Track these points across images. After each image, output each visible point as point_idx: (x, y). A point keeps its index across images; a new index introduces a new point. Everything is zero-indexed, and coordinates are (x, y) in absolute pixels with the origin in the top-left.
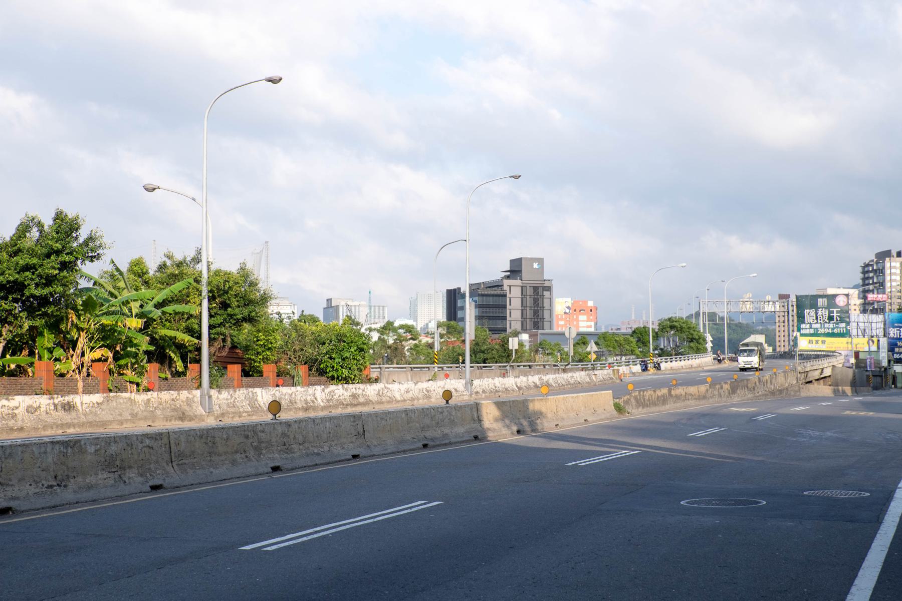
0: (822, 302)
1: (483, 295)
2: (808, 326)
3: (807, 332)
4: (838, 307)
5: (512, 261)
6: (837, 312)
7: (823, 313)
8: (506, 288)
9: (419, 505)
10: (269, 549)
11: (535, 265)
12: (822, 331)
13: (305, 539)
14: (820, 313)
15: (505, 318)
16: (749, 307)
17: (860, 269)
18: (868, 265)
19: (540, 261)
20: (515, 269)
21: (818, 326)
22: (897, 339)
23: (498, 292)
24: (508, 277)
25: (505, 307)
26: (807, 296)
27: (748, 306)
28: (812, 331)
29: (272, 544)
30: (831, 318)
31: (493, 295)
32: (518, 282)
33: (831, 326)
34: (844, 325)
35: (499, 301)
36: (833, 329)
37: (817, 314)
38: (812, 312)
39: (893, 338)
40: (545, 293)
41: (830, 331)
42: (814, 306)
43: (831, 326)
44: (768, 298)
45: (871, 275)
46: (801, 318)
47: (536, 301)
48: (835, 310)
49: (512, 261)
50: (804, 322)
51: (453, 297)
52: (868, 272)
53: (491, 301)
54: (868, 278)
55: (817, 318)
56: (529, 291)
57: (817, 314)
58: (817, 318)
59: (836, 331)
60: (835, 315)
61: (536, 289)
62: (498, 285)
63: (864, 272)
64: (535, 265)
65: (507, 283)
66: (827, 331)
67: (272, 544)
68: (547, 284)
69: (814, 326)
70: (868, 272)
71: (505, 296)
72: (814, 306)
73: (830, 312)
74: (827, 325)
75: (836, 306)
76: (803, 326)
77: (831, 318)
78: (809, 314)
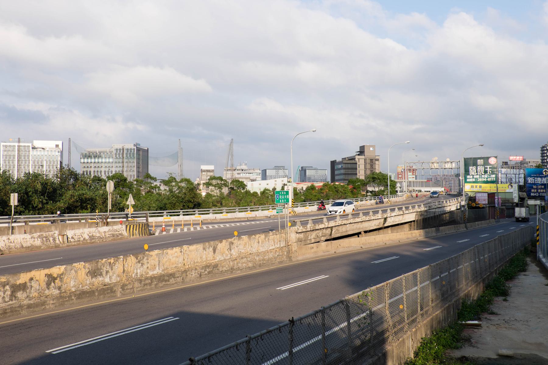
0: (480, 162)
1: (345, 163)
2: (471, 177)
3: (471, 180)
4: (491, 165)
5: (360, 147)
6: (490, 168)
7: (481, 169)
8: (357, 160)
9: (460, 242)
10: (54, 353)
11: (371, 149)
12: (480, 180)
13: (124, 333)
14: (479, 168)
15: (356, 174)
16: (436, 165)
17: (540, 149)
18: (544, 147)
19: (373, 146)
20: (362, 152)
21: (478, 176)
22: (533, 184)
23: (353, 162)
24: (359, 155)
25: (356, 169)
26: (471, 158)
27: (435, 165)
28: (474, 180)
29: (467, 240)
30: (486, 172)
31: (350, 163)
32: (363, 157)
33: (486, 176)
34: (494, 176)
35: (354, 166)
36: (487, 178)
37: (477, 169)
38: (474, 168)
39: (530, 184)
40: (376, 162)
41: (485, 180)
42: (475, 164)
43: (486, 176)
44: (448, 160)
45: (545, 152)
46: (467, 172)
47: (372, 166)
48: (488, 167)
49: (360, 147)
50: (469, 174)
51: (333, 163)
52: (544, 150)
53: (349, 166)
54: (544, 153)
55: (477, 172)
56: (368, 161)
57: (477, 169)
58: (477, 172)
59: (489, 180)
60: (488, 169)
61: (371, 160)
62: (353, 159)
63: (542, 150)
64: (371, 149)
65: (357, 157)
66: (483, 180)
67: (467, 240)
68: (377, 158)
69: (475, 177)
70: (544, 150)
71: (356, 163)
72: (475, 164)
73: (485, 168)
74: (483, 176)
75: (489, 164)
76: (468, 177)
77: (486, 172)
78: (472, 169)
